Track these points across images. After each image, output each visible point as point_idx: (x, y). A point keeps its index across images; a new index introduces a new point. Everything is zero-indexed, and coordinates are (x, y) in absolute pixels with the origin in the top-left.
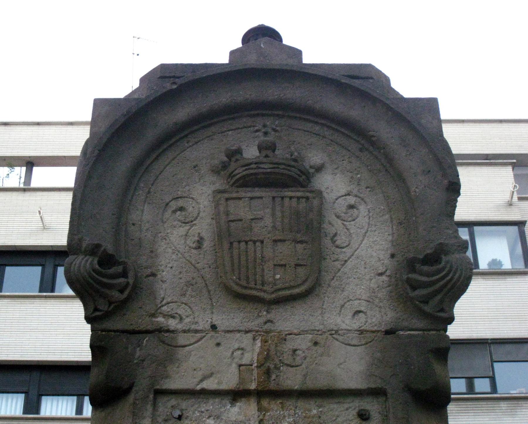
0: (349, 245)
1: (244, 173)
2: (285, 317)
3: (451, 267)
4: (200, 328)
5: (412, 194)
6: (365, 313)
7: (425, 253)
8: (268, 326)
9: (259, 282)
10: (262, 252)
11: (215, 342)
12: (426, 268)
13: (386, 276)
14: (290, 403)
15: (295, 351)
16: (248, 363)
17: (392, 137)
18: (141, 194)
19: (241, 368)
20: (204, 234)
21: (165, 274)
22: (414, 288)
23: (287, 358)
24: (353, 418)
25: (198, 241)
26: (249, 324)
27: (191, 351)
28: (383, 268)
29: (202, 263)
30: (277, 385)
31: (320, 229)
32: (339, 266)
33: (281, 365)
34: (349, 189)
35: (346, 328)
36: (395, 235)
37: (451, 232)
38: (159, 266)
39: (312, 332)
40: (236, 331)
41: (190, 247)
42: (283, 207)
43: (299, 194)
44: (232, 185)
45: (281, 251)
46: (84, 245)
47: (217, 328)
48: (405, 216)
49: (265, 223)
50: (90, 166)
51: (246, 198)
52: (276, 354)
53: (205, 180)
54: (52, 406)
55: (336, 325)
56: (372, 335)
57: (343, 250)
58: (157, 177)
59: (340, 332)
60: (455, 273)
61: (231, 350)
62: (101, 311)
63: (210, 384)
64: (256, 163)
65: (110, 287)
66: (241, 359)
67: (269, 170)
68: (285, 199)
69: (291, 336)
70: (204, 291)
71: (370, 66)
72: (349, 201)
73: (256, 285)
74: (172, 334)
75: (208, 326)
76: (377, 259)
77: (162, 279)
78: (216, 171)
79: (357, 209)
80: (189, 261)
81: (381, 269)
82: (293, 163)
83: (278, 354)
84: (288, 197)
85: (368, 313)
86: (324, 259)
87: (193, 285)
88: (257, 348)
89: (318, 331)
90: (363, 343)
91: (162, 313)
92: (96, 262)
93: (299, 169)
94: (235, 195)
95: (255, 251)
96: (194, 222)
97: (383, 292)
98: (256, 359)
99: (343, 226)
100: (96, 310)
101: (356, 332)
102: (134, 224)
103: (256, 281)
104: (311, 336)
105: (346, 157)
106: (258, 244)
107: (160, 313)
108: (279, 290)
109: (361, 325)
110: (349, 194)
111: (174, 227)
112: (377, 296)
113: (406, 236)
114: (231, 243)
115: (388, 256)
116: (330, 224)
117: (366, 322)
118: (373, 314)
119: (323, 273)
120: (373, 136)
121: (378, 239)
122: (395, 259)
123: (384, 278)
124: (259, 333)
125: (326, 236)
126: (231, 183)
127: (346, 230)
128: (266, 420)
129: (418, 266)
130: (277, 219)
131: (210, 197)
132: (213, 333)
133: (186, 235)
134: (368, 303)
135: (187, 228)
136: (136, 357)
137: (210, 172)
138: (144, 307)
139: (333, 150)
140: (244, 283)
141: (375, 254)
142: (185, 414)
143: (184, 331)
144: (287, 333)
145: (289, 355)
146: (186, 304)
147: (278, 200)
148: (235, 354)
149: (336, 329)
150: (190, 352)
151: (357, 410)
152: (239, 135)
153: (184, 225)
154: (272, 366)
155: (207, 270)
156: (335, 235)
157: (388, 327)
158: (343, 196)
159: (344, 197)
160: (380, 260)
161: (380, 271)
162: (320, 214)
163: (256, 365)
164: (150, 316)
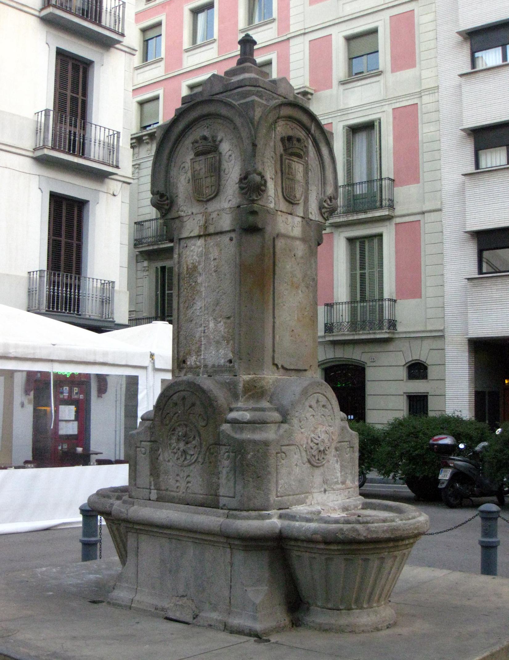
14: (213, 237)
15: (213, 218)
18: (173, 164)
21: (180, 195)
54: (500, 157)
63: (192, 235)
65: (164, 204)
100: (163, 213)
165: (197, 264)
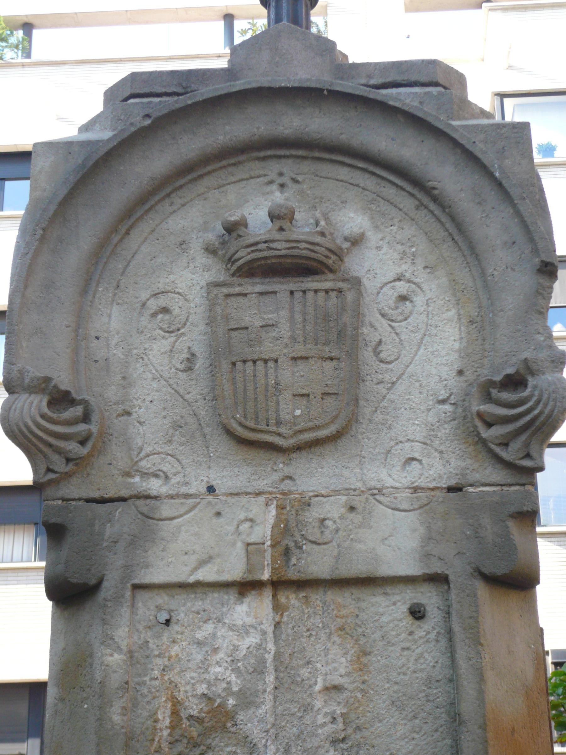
0: (398, 358)
1: (249, 257)
2: (309, 471)
3: (541, 391)
4: (192, 491)
5: (489, 278)
6: (420, 461)
7: (504, 373)
8: (287, 485)
9: (272, 422)
10: (276, 377)
11: (214, 511)
12: (506, 396)
13: (451, 404)
16: (258, 541)
17: (462, 190)
19: (250, 548)
20: (196, 349)
22: (489, 425)
23: (313, 533)
24: (402, 616)
25: (188, 359)
26: (259, 482)
27: (180, 526)
28: (446, 393)
29: (194, 393)
30: (299, 572)
31: (355, 337)
32: (384, 392)
33: (304, 542)
34: (399, 271)
35: (393, 485)
36: (465, 340)
37: (542, 339)
38: (134, 401)
39: (347, 492)
40: (242, 493)
41: (177, 369)
42: (304, 305)
43: (328, 285)
44: (233, 275)
45: (302, 374)
46: (27, 381)
47: (215, 490)
48: (478, 310)
49: (280, 332)
50: (30, 256)
51: (253, 293)
52: (297, 525)
53: (196, 265)
55: (379, 481)
56: (429, 493)
57: (390, 366)
58: (130, 262)
59: (384, 491)
60: (546, 405)
61: (235, 523)
62: (54, 472)
64: (266, 242)
66: (249, 535)
67: (283, 252)
68: (307, 293)
69: (317, 499)
70: (198, 434)
71: (434, 63)
72: (400, 290)
73: (268, 426)
74: (153, 502)
75: (203, 489)
76: (437, 378)
77: (139, 420)
78: (210, 250)
79: (411, 302)
80: (176, 391)
81: (443, 395)
82: (318, 239)
83: (300, 527)
84: (312, 290)
85: (424, 462)
86: (363, 381)
87: (181, 427)
88: (270, 517)
89: (355, 490)
90: (416, 507)
91: (140, 471)
92: (45, 403)
93: (326, 248)
94: (237, 290)
95: (266, 374)
96: (182, 331)
97: (446, 429)
98: (270, 534)
99: (390, 329)
100: (49, 470)
101: (407, 490)
102: (97, 338)
103: (267, 419)
104: (344, 498)
105: (396, 221)
106: (271, 364)
107: (138, 471)
108: (301, 432)
109: (413, 480)
110: (399, 279)
111: (155, 339)
112: (437, 435)
113: (480, 342)
114: (234, 364)
115: (454, 373)
116: (372, 326)
117: (421, 474)
118: (431, 463)
119: (362, 403)
120: (434, 188)
121: (439, 347)
122: (463, 378)
123: (448, 407)
124: (274, 496)
125: (366, 345)
126: (232, 271)
127: (394, 335)
128: (284, 623)
129: (494, 392)
130: (297, 326)
131: (203, 290)
132: (210, 498)
133: (172, 351)
134: (424, 446)
135: (172, 340)
136: (106, 538)
137: (203, 251)
138: (114, 462)
139: (378, 209)
140: (251, 424)
141: (434, 371)
142: (174, 620)
143: (172, 497)
144: (312, 494)
145: (314, 527)
146: (172, 456)
147: (298, 295)
148: (241, 528)
149: (379, 486)
150: (179, 527)
151: (408, 606)
152: (243, 191)
153: (167, 334)
154: (292, 545)
155: (201, 403)
156: (380, 342)
157: (453, 482)
158: (391, 282)
159: (392, 284)
160: (441, 381)
161: (441, 398)
162: (358, 314)
163: (269, 543)
164: (123, 476)
165: (231, 702)
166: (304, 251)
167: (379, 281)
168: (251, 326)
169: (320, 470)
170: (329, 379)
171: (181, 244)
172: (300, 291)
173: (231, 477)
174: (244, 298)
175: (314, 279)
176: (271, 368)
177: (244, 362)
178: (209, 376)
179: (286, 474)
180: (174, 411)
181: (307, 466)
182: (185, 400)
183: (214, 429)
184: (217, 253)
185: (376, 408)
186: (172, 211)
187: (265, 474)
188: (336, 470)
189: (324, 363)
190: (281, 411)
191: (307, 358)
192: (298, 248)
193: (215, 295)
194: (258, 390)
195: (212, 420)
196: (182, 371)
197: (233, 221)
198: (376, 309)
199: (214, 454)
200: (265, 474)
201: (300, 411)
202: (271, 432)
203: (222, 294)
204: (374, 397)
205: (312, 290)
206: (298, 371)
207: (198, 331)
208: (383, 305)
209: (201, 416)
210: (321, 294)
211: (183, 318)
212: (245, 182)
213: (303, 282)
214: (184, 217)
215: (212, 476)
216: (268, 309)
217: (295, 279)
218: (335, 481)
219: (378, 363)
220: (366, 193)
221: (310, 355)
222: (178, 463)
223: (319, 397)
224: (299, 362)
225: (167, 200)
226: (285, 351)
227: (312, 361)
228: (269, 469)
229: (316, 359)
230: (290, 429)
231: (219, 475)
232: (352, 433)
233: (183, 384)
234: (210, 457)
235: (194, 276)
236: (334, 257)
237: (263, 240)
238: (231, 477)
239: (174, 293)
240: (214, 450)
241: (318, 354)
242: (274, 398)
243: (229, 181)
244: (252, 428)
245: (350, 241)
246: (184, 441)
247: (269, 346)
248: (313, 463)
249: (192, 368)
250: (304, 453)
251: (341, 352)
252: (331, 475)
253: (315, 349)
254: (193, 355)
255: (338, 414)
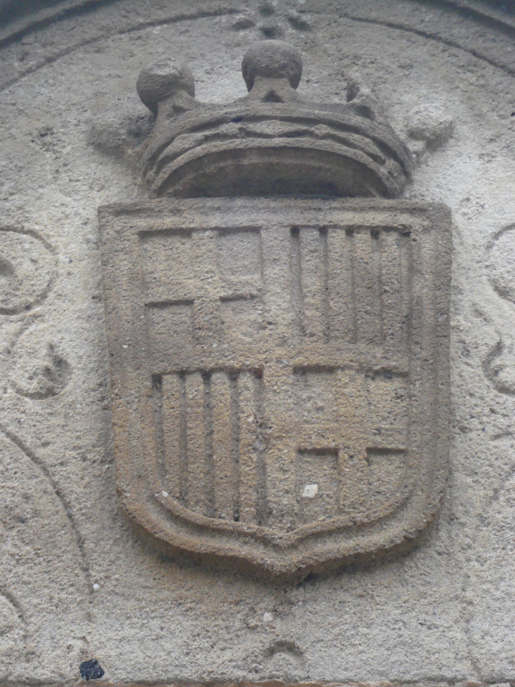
1: (199, 150)
2: (336, 631)
9: (248, 510)
25: (47, 371)
42: (326, 258)
44: (160, 192)
47: (102, 673)
49: (268, 311)
51: (205, 230)
53: (75, 177)
64: (237, 120)
68: (331, 233)
73: (237, 519)
80: (14, 439)
82: (356, 120)
84: (341, 228)
86: (463, 430)
96: (37, 309)
103: (237, 504)
133: (9, 352)
139: (482, 82)
156: (499, 348)
166: (322, 142)
167: (491, 221)
168: (199, 298)
169: (363, 630)
170: (384, 419)
171: (42, 136)
172: (314, 227)
173: (141, 641)
174: (184, 241)
175: (348, 204)
176: (247, 389)
177: (183, 374)
178: (95, 407)
179: (280, 638)
180: (9, 484)
181: (332, 619)
182: (35, 460)
183: (104, 528)
184: (123, 152)
185: (496, 491)
186: (24, 70)
187: (227, 637)
188: (405, 632)
189: (370, 381)
190: (269, 484)
191: (331, 370)
192: (311, 134)
193: (118, 232)
194: (215, 436)
195: (99, 506)
196: (32, 396)
197: (164, 77)
198: (484, 278)
199: (102, 586)
200: (227, 637)
201: (315, 487)
202: (246, 535)
203: (133, 231)
204: (491, 466)
205: (341, 228)
206: (310, 398)
207: (75, 312)
208: (503, 269)
209: (74, 496)
210: (364, 237)
211: (40, 286)
212: (188, 22)
213: (320, 209)
214: (51, 81)
215: (94, 639)
216: (239, 263)
217: (301, 203)
218: (402, 658)
219: (495, 392)
220: (454, 50)
221: (340, 362)
222: (11, 605)
223: (361, 457)
224: (313, 379)
225: (14, 48)
226: (279, 351)
227: (343, 377)
228: (238, 624)
229: (353, 373)
230: (290, 529)
231: (111, 634)
232: (439, 546)
233: (32, 423)
234: (92, 591)
235: (69, 199)
236: (391, 163)
237: (234, 116)
238: (141, 641)
239: (23, 231)
240: (102, 575)
241: (357, 361)
242: (254, 456)
243: (153, 18)
244: (199, 522)
245: (423, 138)
246: (29, 552)
247: (242, 342)
248: (346, 613)
249: (57, 390)
250: (324, 589)
251: (411, 359)
252: (392, 642)
253: (350, 350)
254: (60, 362)
255: (407, 499)
